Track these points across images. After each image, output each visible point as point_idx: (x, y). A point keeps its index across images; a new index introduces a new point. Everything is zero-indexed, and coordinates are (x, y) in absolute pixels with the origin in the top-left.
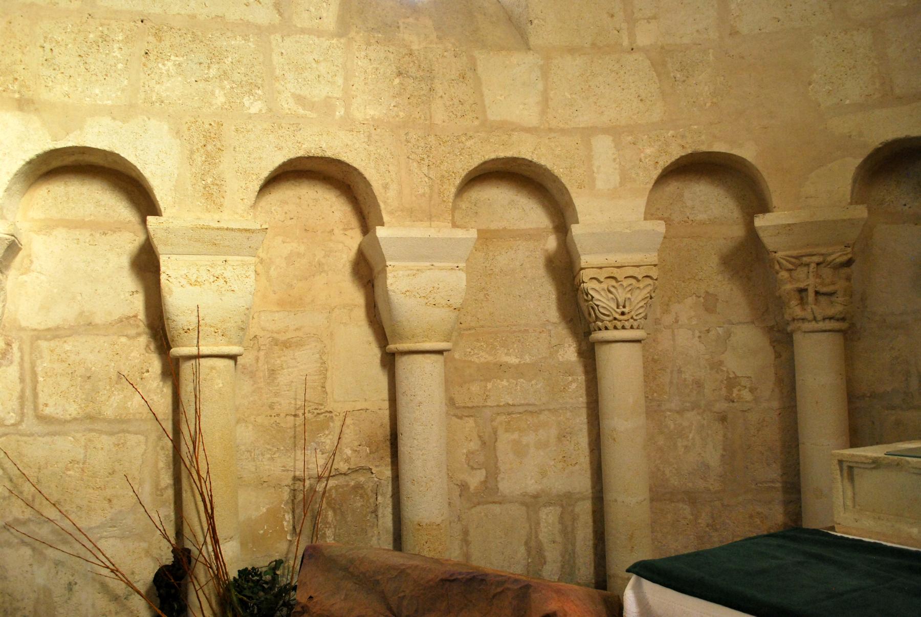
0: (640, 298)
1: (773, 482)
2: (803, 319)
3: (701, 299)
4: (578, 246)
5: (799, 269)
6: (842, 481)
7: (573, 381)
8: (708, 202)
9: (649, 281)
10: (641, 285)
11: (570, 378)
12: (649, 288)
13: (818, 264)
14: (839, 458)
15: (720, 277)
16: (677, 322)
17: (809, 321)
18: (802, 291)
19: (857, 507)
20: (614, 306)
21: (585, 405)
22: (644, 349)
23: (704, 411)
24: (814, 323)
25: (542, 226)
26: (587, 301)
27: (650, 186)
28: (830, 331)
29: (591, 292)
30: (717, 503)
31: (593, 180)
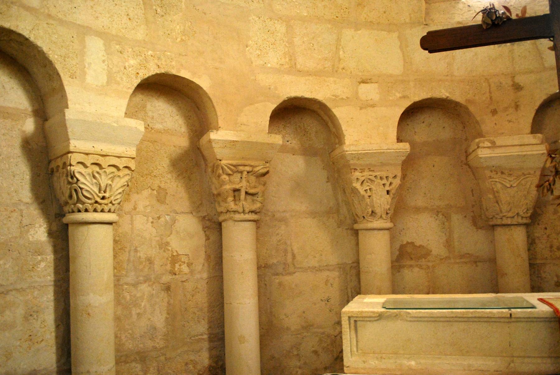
0: (119, 185)
1: (202, 335)
2: (234, 212)
3: (155, 191)
4: (69, 130)
5: (235, 174)
6: (350, 331)
7: (42, 260)
8: (166, 115)
9: (127, 171)
10: (121, 174)
11: (39, 258)
12: (127, 178)
13: (248, 172)
14: (350, 315)
15: (169, 176)
16: (135, 209)
17: (239, 213)
18: (236, 191)
19: (360, 351)
20: (96, 190)
21: (52, 283)
22: (115, 230)
23: (154, 283)
24: (242, 214)
25: (21, 107)
26: (69, 183)
27: (131, 91)
28: (250, 221)
29: (78, 175)
30: (162, 358)
31: (85, 73)
